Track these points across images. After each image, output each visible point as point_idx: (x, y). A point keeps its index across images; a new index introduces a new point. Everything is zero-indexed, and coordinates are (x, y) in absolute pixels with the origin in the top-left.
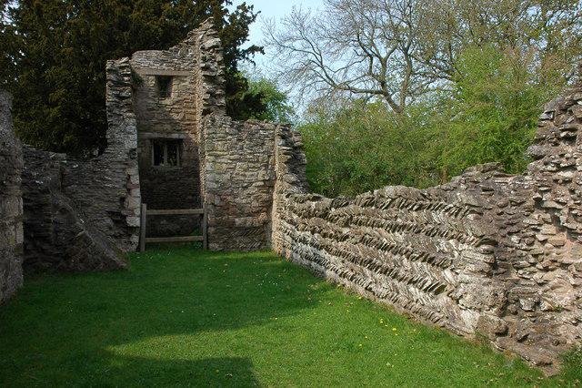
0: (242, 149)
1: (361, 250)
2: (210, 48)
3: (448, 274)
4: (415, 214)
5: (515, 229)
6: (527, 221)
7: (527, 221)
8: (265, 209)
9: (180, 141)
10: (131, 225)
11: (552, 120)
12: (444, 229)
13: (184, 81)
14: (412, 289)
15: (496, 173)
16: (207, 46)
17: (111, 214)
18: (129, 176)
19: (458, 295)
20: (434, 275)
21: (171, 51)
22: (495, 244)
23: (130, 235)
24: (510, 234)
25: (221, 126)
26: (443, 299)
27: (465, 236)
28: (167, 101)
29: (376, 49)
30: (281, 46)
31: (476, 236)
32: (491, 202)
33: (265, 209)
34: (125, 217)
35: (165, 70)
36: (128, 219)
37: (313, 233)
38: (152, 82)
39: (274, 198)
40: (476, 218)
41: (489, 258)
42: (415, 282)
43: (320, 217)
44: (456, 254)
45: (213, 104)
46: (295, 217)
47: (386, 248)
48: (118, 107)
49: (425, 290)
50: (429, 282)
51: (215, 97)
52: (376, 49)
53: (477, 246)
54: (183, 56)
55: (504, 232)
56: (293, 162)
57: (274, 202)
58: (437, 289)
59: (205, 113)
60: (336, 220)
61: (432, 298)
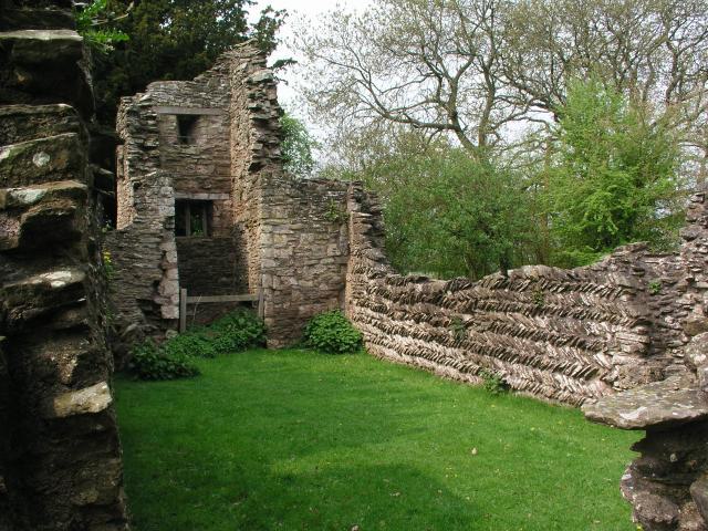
0: (306, 215)
1: (490, 339)
2: (259, 82)
3: (600, 357)
4: (560, 296)
5: (668, 308)
6: (680, 301)
7: (680, 301)
8: (336, 293)
9: (209, 203)
10: (168, 316)
11: (702, 203)
12: (595, 311)
13: (214, 122)
14: (558, 376)
15: (646, 253)
16: (255, 79)
17: (142, 302)
18: (165, 252)
19: (613, 377)
20: (585, 359)
21: (198, 81)
22: (648, 324)
23: (165, 331)
24: (664, 314)
25: (279, 186)
26: (595, 385)
27: (618, 317)
28: (191, 150)
29: (443, 66)
30: (312, 55)
31: (631, 317)
32: (643, 283)
33: (336, 293)
34: (159, 306)
35: (189, 108)
36: (164, 309)
37: (417, 321)
38: (173, 124)
39: (348, 278)
40: (629, 300)
41: (644, 339)
42: (562, 369)
43: (429, 301)
44: (609, 336)
45: (265, 156)
46: (388, 303)
47: (524, 335)
48: (141, 160)
49: (575, 377)
50: (580, 367)
51: (267, 146)
52: (443, 66)
53: (632, 327)
54: (213, 89)
55: (656, 313)
56: (374, 233)
57: (348, 285)
58: (588, 375)
59: (255, 168)
60: (453, 306)
61: (583, 384)
